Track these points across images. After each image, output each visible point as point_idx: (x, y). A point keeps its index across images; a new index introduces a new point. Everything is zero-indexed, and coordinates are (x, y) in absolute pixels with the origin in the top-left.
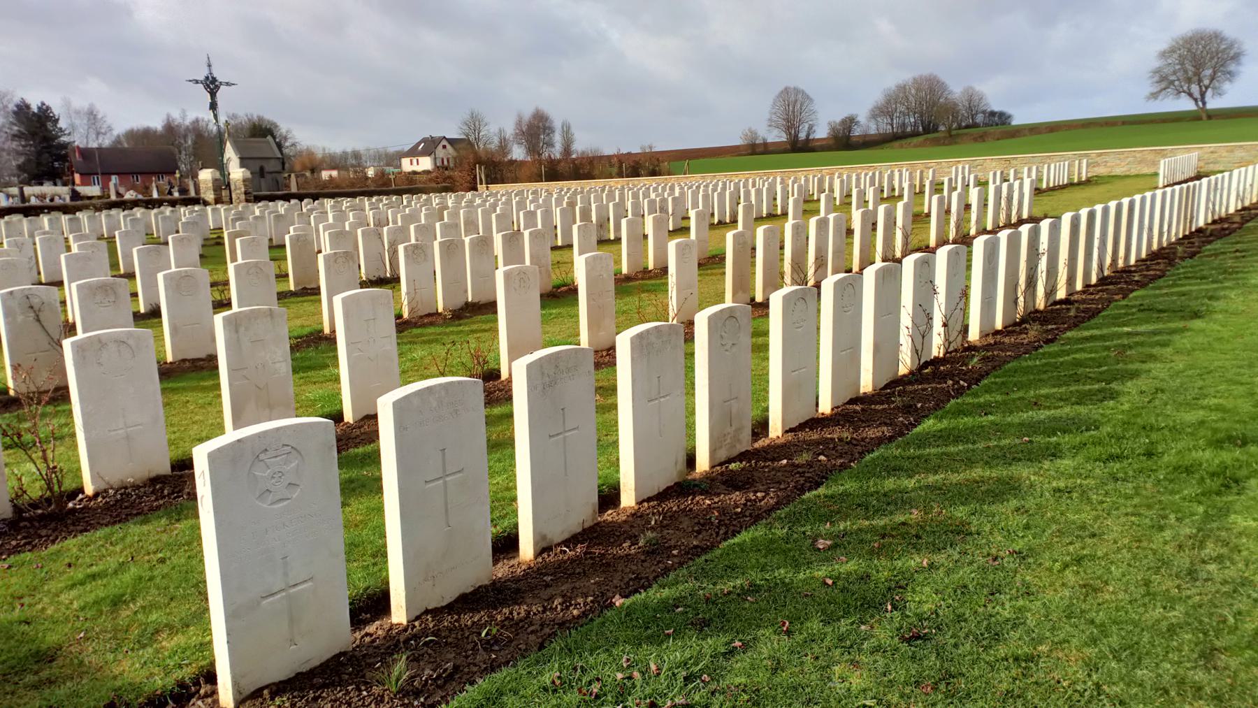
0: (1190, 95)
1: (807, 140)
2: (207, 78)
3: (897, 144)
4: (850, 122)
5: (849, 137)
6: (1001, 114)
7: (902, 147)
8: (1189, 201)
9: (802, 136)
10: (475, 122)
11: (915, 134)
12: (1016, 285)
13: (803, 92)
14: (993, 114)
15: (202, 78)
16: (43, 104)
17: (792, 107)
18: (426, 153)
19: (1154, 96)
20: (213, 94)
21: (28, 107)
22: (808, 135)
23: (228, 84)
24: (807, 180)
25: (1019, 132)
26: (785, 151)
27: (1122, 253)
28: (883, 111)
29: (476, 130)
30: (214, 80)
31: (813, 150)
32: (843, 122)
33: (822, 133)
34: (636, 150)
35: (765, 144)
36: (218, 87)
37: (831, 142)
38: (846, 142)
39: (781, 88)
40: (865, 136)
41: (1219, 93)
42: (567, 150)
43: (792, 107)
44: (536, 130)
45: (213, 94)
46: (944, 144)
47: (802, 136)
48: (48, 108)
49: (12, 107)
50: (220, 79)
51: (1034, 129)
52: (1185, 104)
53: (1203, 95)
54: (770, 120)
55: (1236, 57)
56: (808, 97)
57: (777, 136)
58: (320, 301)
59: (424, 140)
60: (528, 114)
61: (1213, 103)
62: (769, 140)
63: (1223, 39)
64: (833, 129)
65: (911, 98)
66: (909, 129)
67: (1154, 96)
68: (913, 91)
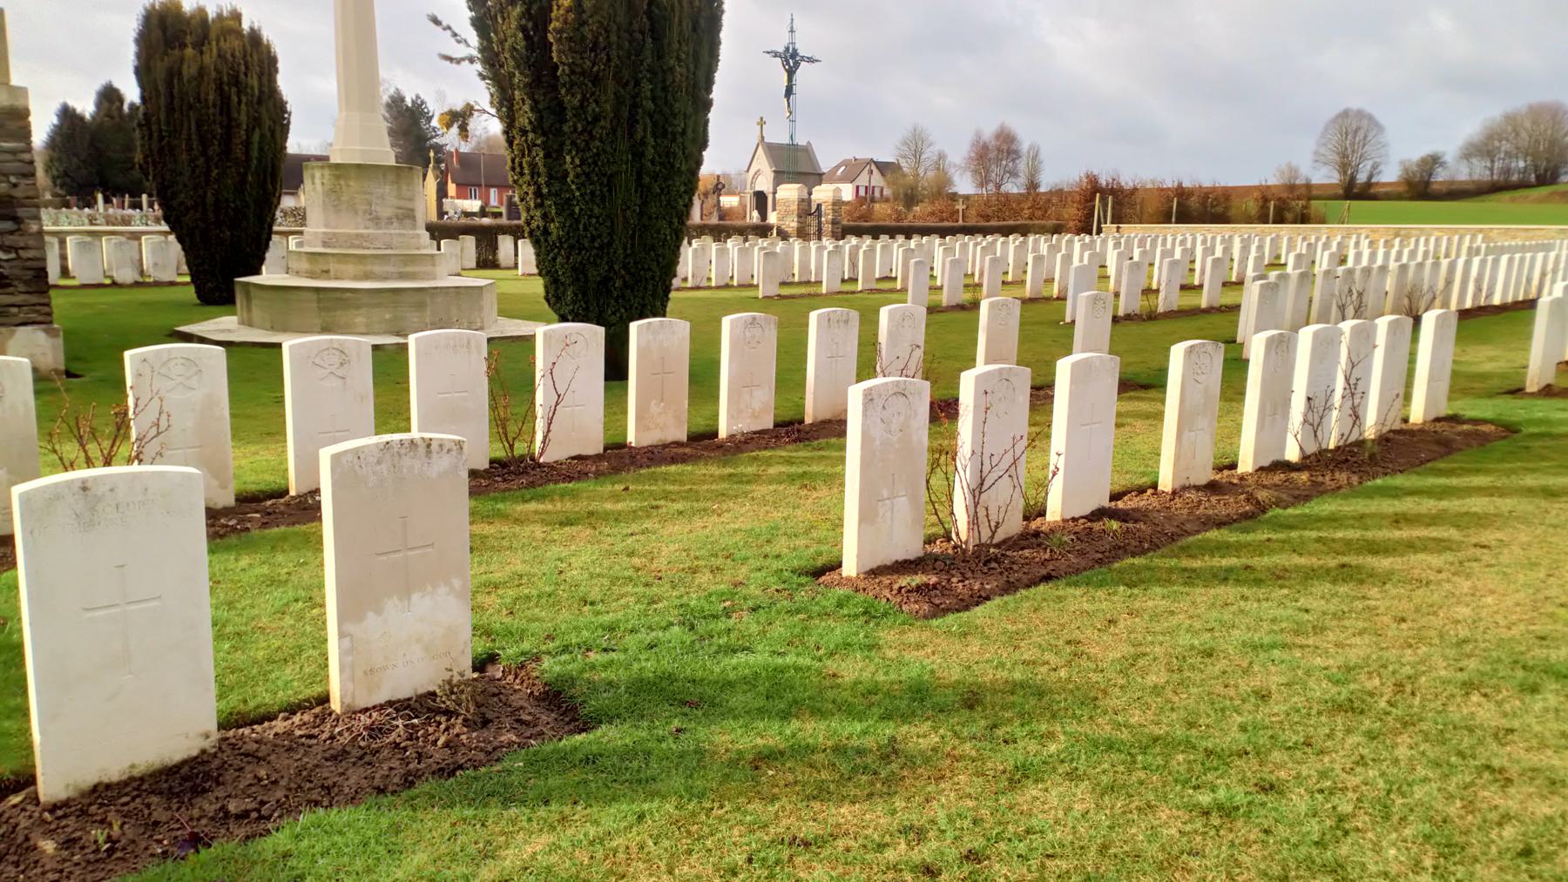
1: (1369, 184)
2: (787, 49)
3: (1507, 195)
4: (1433, 161)
5: (1427, 183)
7: (1513, 200)
9: (1362, 178)
11: (1523, 185)
12: (1287, 393)
15: (781, 49)
16: (418, 97)
17: (1352, 132)
18: (849, 178)
20: (791, 73)
21: (403, 99)
22: (1371, 177)
23: (811, 60)
24: (1227, 250)
26: (1336, 197)
28: (1482, 149)
29: (917, 154)
30: (794, 54)
31: (1374, 198)
32: (1424, 161)
33: (1390, 174)
34: (1207, 184)
35: (1308, 186)
36: (797, 65)
37: (1401, 189)
38: (1422, 188)
39: (1341, 109)
40: (1452, 182)
42: (1033, 185)
43: (1352, 132)
44: (997, 152)
45: (791, 73)
47: (1362, 178)
48: (423, 102)
49: (385, 98)
50: (801, 52)
54: (1316, 153)
57: (1325, 176)
59: (845, 163)
60: (989, 132)
62: (1314, 181)
64: (1406, 170)
65: (1524, 135)
66: (1515, 178)
68: (1528, 124)
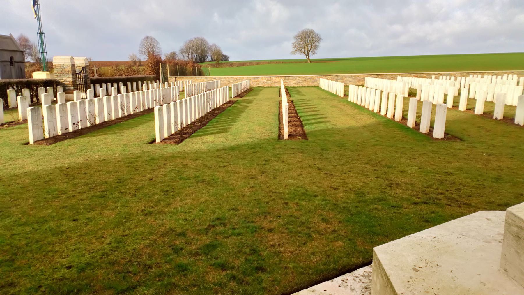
0: (304, 53)
6: (225, 56)
8: (209, 100)
10: (149, 44)
13: (154, 39)
14: (223, 56)
19: (293, 53)
25: (232, 64)
27: (179, 123)
32: (171, 54)
41: (314, 53)
46: (216, 67)
51: (242, 64)
52: (303, 57)
53: (308, 54)
54: (139, 50)
55: (318, 41)
56: (157, 42)
58: (27, 128)
61: (312, 57)
63: (315, 33)
67: (293, 53)
